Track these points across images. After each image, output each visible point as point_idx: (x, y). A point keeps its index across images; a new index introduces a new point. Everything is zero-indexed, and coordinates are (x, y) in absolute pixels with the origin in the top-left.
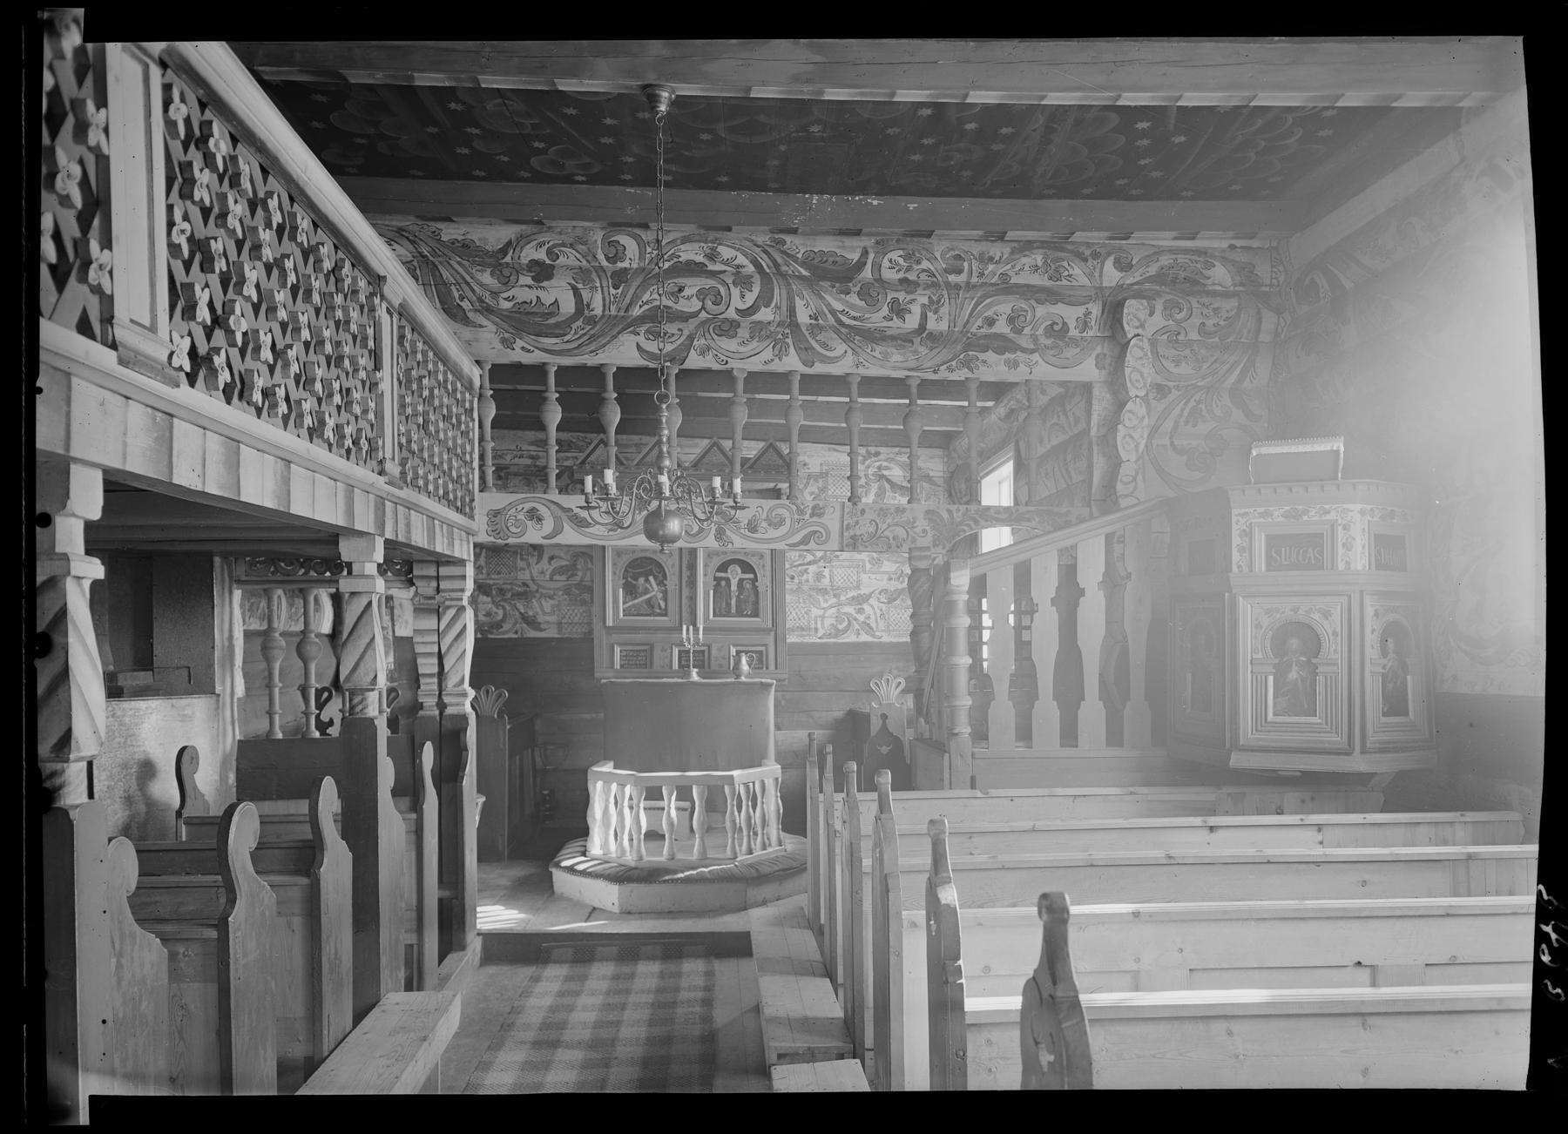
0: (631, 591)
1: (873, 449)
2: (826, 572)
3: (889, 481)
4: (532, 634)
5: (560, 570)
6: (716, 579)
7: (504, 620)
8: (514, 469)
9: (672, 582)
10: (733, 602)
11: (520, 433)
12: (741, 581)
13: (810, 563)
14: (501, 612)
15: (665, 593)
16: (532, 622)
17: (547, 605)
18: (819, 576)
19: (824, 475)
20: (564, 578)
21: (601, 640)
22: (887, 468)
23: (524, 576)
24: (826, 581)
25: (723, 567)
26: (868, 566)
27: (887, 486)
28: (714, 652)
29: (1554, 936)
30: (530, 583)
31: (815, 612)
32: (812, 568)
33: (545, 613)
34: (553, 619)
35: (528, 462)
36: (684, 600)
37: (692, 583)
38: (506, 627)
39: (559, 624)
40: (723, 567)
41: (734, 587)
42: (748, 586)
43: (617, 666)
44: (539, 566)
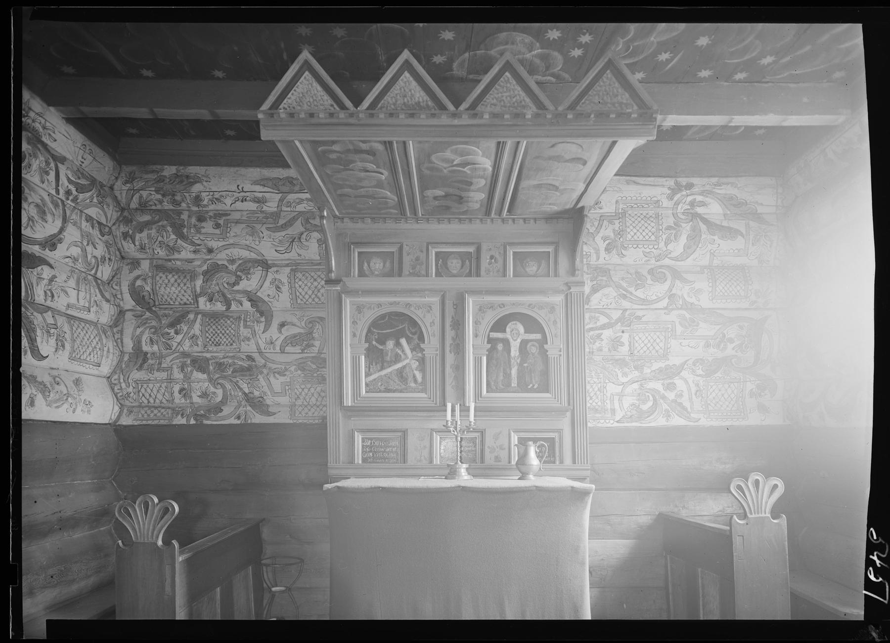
0: (376, 357)
1: (683, 181)
2: (625, 338)
3: (705, 221)
4: (258, 419)
5: (293, 340)
6: (490, 340)
7: (224, 402)
8: (236, 216)
9: (431, 346)
10: (514, 372)
11: (243, 171)
12: (524, 344)
13: (604, 327)
14: (220, 392)
15: (422, 361)
16: (258, 404)
17: (277, 383)
18: (616, 343)
19: (620, 216)
20: (298, 349)
21: (340, 428)
22: (703, 204)
23: (249, 347)
24: (625, 349)
25: (500, 325)
26: (679, 329)
27: (703, 227)
28: (489, 441)
29: (878, 562)
30: (256, 356)
31: (612, 388)
32: (607, 333)
33: (275, 394)
34: (284, 400)
35: (253, 206)
36: (448, 370)
37: (459, 348)
38: (227, 410)
39: (292, 406)
40: (500, 325)
41: (514, 352)
42: (533, 349)
43: (359, 460)
44: (267, 335)
